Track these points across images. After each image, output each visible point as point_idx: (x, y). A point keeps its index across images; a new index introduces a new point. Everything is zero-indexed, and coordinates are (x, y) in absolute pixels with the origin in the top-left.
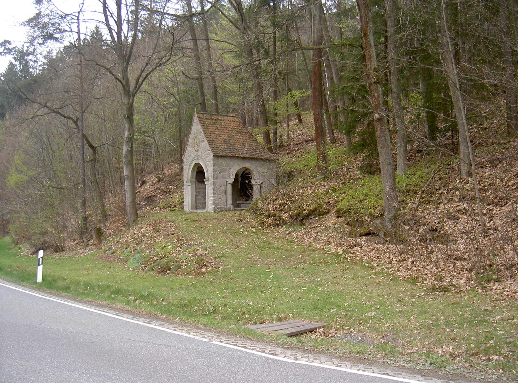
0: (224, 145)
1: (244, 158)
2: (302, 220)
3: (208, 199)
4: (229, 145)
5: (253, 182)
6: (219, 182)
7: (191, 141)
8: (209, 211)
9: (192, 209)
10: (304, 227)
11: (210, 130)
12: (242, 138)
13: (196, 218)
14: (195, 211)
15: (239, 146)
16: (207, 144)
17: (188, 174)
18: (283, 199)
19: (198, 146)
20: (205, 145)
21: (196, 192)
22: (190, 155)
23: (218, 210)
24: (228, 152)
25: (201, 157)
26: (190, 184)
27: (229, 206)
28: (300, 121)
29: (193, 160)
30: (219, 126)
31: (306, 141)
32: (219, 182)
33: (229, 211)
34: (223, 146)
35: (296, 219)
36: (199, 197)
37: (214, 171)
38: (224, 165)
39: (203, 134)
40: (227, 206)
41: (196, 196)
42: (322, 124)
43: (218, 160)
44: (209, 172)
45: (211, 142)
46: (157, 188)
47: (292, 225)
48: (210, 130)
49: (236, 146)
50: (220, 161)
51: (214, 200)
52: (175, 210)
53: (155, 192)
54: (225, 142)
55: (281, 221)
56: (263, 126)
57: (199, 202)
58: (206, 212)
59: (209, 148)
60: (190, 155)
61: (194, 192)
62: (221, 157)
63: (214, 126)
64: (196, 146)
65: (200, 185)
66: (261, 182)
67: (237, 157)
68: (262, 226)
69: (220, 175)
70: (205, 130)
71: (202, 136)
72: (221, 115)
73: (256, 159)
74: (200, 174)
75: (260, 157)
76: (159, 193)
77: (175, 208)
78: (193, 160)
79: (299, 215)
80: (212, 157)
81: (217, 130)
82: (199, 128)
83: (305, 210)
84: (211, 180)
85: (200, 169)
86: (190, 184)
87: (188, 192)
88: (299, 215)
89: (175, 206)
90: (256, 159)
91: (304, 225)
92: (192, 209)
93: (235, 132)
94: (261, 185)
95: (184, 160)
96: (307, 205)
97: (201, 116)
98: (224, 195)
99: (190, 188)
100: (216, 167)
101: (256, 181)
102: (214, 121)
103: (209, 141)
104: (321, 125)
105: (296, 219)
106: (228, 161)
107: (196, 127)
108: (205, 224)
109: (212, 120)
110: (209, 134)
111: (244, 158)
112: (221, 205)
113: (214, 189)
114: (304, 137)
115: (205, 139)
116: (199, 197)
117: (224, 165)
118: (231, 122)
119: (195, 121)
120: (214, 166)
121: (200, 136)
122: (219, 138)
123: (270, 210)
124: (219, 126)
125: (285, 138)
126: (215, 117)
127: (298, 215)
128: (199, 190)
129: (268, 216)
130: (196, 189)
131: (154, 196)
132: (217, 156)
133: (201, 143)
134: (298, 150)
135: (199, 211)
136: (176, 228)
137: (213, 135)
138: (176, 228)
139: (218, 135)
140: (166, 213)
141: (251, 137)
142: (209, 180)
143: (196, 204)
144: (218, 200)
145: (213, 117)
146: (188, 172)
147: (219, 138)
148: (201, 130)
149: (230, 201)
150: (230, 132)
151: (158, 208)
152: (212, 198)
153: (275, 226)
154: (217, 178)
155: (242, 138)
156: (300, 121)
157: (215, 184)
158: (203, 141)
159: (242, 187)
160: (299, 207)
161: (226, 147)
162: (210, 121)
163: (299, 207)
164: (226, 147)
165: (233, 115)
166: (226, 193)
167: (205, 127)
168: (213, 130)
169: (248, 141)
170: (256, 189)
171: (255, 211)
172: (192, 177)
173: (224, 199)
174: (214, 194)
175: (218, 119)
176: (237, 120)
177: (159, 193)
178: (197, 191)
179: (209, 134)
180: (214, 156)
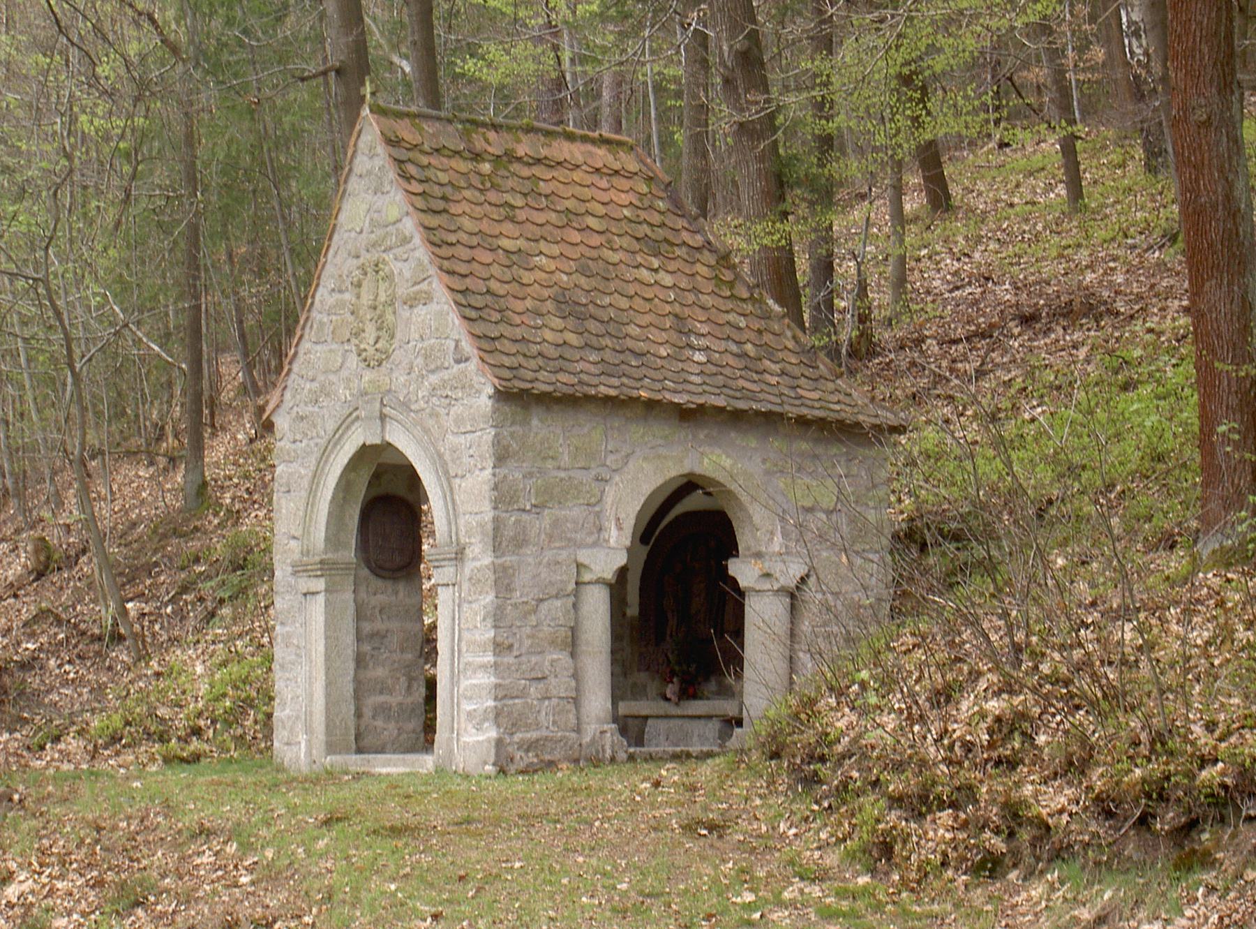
0: (557, 323)
1: (689, 415)
2: (1191, 826)
3: (454, 680)
4: (593, 326)
5: (743, 571)
6: (532, 568)
7: (327, 300)
8: (461, 761)
9: (331, 748)
10: (1209, 877)
11: (467, 223)
12: (668, 280)
13: (395, 813)
14: (355, 762)
15: (654, 334)
16: (454, 319)
17: (303, 513)
18: (1008, 688)
19: (386, 330)
20: (436, 320)
21: (359, 638)
22: (325, 391)
23: (524, 758)
24: (584, 372)
25: (406, 406)
26: (320, 584)
27: (590, 730)
28: (940, 199)
29: (345, 425)
30: (519, 201)
31: (1028, 320)
32: (532, 568)
33: (596, 762)
34: (553, 331)
35: (1144, 821)
36: (380, 672)
37: (503, 496)
38: (566, 459)
39: (421, 252)
40: (578, 730)
41: (360, 661)
42: (1230, 185)
43: (525, 422)
44: (458, 504)
45: (478, 301)
46: (42, 615)
47: (1108, 865)
48: (467, 223)
49: (633, 330)
50: (540, 426)
51: (502, 694)
52: (196, 758)
53: (32, 636)
54: (566, 305)
55: (1025, 835)
56: (762, 217)
57: (396, 696)
58: (440, 771)
59: (468, 346)
60: (325, 391)
61: (349, 639)
62: (548, 401)
63: (493, 196)
64: (370, 332)
65: (384, 594)
66: (796, 570)
67: (651, 405)
68: (873, 871)
69: (539, 525)
70: (434, 221)
71: (413, 260)
72: (529, 130)
73: (769, 421)
74: (388, 513)
75: (793, 412)
76: (55, 648)
77: (195, 744)
78: (345, 425)
79: (1163, 797)
80: (484, 401)
81: (507, 227)
82: (394, 213)
83: (1204, 762)
84: (480, 557)
85: (401, 490)
86: (320, 584)
87: (306, 644)
88: (1163, 797)
89: (197, 732)
90: (769, 421)
91: (1206, 860)
92: (331, 748)
93: (625, 242)
94: (794, 596)
95: (282, 422)
96: (1210, 726)
97: (404, 130)
98: (563, 657)
99: (318, 607)
100: (514, 472)
101: (761, 567)
102: (486, 167)
103: (466, 301)
104: (1228, 197)
105: (1144, 821)
106: (589, 430)
107: (372, 207)
108: (473, 855)
109: (477, 157)
110: (465, 253)
111: (689, 415)
112: (546, 723)
113: (498, 617)
114: (1004, 292)
115: (438, 287)
116: (380, 672)
117: (566, 459)
118: (599, 180)
119: (362, 163)
120: (501, 457)
121: (396, 267)
122: (527, 277)
123: (923, 763)
124: (519, 201)
125: (880, 297)
126: (495, 143)
127: (1158, 792)
128: (380, 626)
129: (920, 805)
130: (360, 616)
131: (25, 666)
132: (516, 398)
133: (405, 312)
134: (981, 373)
135: (390, 766)
136: (270, 876)
137: (486, 257)
138: (270, 876)
139: (517, 258)
140: (140, 777)
141: (728, 276)
142: (459, 555)
143: (359, 715)
144: (523, 694)
145: (479, 144)
146: (311, 502)
147: (527, 277)
148: (409, 225)
149: (598, 701)
150: (596, 240)
151: (72, 743)
152: (486, 680)
153: (976, 869)
154: (520, 542)
155: (668, 280)
156: (940, 199)
157: (503, 580)
158: (427, 298)
159: (680, 608)
160: (1159, 739)
161: (572, 338)
162: (463, 166)
163: (1159, 739)
164: (572, 338)
165: (702, 94)
166: (572, 643)
167: (433, 206)
168: (485, 226)
169: (708, 300)
170: (763, 616)
171: (805, 763)
172: (333, 540)
173: (561, 685)
174: (500, 647)
175: (511, 156)
176: (633, 166)
177: (55, 648)
178: (367, 627)
179: (465, 253)
180: (504, 396)
